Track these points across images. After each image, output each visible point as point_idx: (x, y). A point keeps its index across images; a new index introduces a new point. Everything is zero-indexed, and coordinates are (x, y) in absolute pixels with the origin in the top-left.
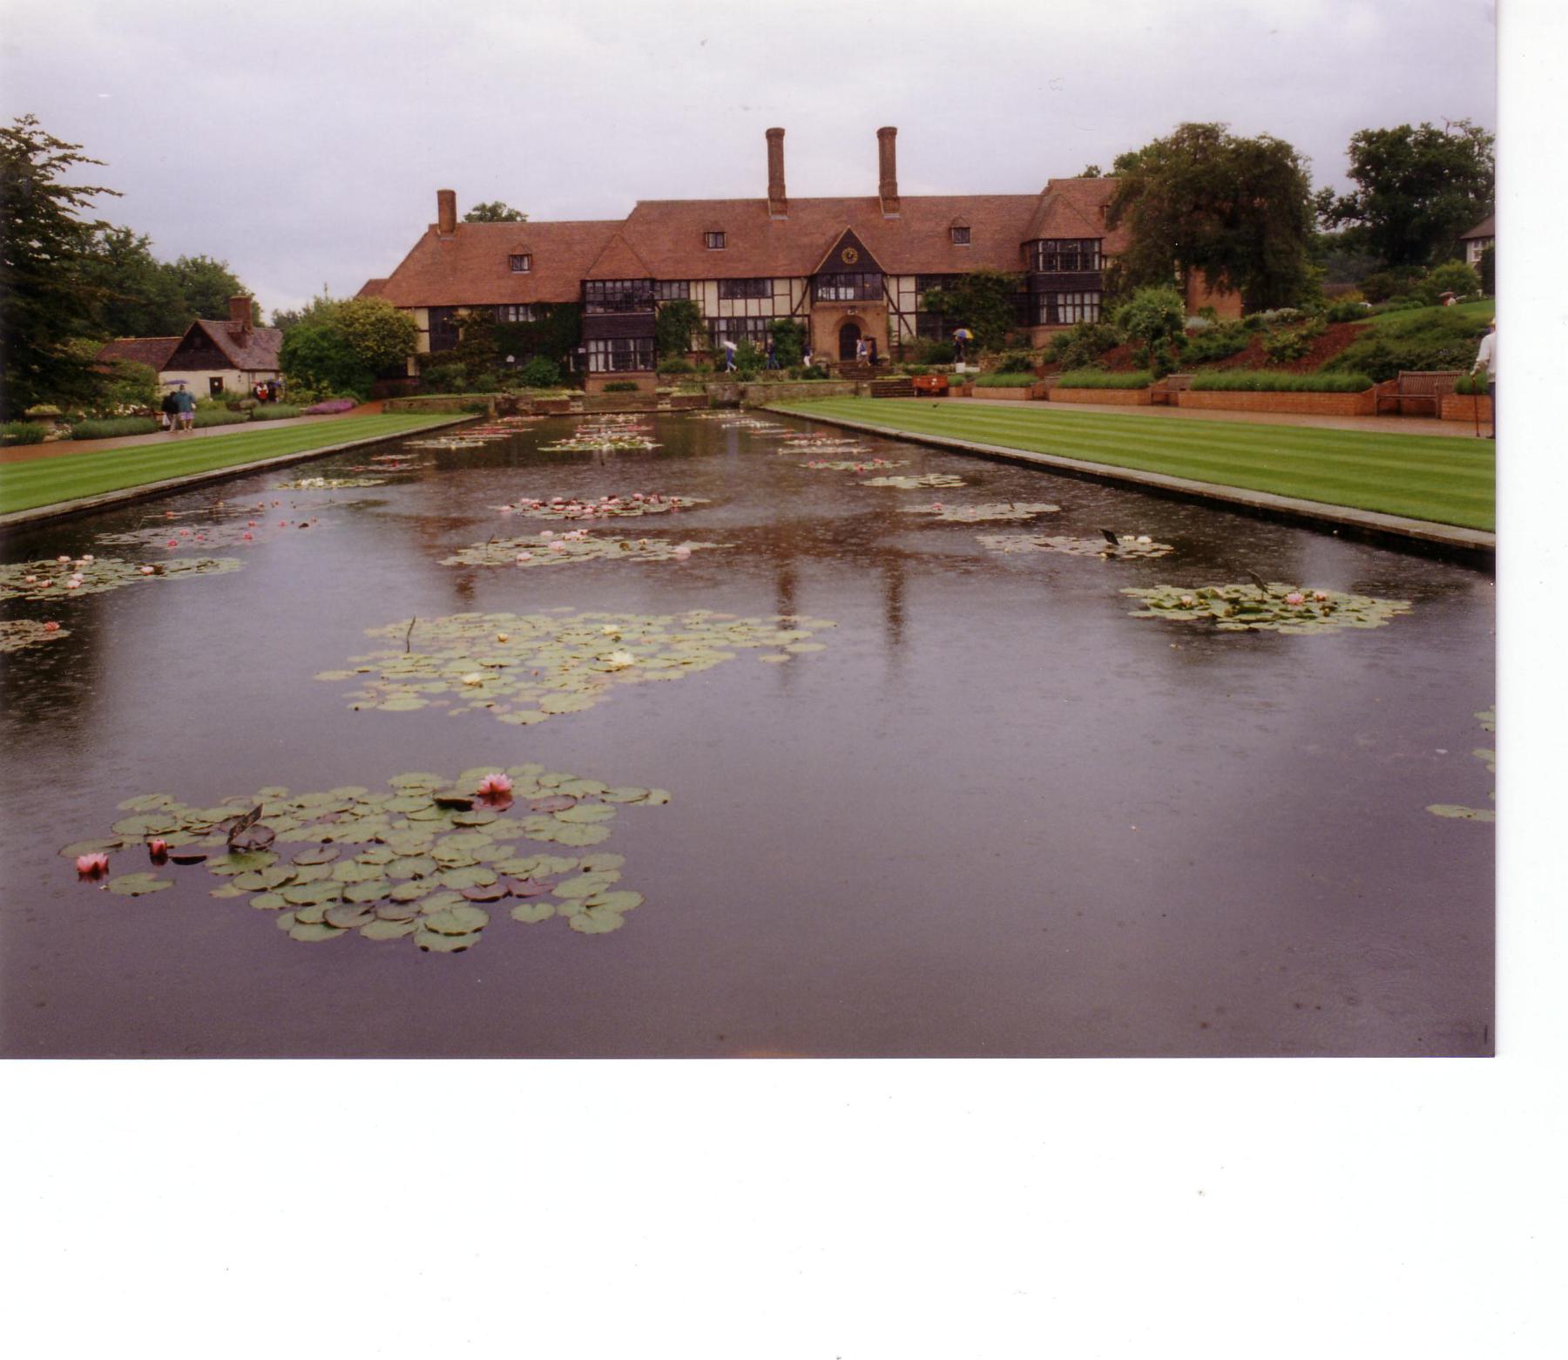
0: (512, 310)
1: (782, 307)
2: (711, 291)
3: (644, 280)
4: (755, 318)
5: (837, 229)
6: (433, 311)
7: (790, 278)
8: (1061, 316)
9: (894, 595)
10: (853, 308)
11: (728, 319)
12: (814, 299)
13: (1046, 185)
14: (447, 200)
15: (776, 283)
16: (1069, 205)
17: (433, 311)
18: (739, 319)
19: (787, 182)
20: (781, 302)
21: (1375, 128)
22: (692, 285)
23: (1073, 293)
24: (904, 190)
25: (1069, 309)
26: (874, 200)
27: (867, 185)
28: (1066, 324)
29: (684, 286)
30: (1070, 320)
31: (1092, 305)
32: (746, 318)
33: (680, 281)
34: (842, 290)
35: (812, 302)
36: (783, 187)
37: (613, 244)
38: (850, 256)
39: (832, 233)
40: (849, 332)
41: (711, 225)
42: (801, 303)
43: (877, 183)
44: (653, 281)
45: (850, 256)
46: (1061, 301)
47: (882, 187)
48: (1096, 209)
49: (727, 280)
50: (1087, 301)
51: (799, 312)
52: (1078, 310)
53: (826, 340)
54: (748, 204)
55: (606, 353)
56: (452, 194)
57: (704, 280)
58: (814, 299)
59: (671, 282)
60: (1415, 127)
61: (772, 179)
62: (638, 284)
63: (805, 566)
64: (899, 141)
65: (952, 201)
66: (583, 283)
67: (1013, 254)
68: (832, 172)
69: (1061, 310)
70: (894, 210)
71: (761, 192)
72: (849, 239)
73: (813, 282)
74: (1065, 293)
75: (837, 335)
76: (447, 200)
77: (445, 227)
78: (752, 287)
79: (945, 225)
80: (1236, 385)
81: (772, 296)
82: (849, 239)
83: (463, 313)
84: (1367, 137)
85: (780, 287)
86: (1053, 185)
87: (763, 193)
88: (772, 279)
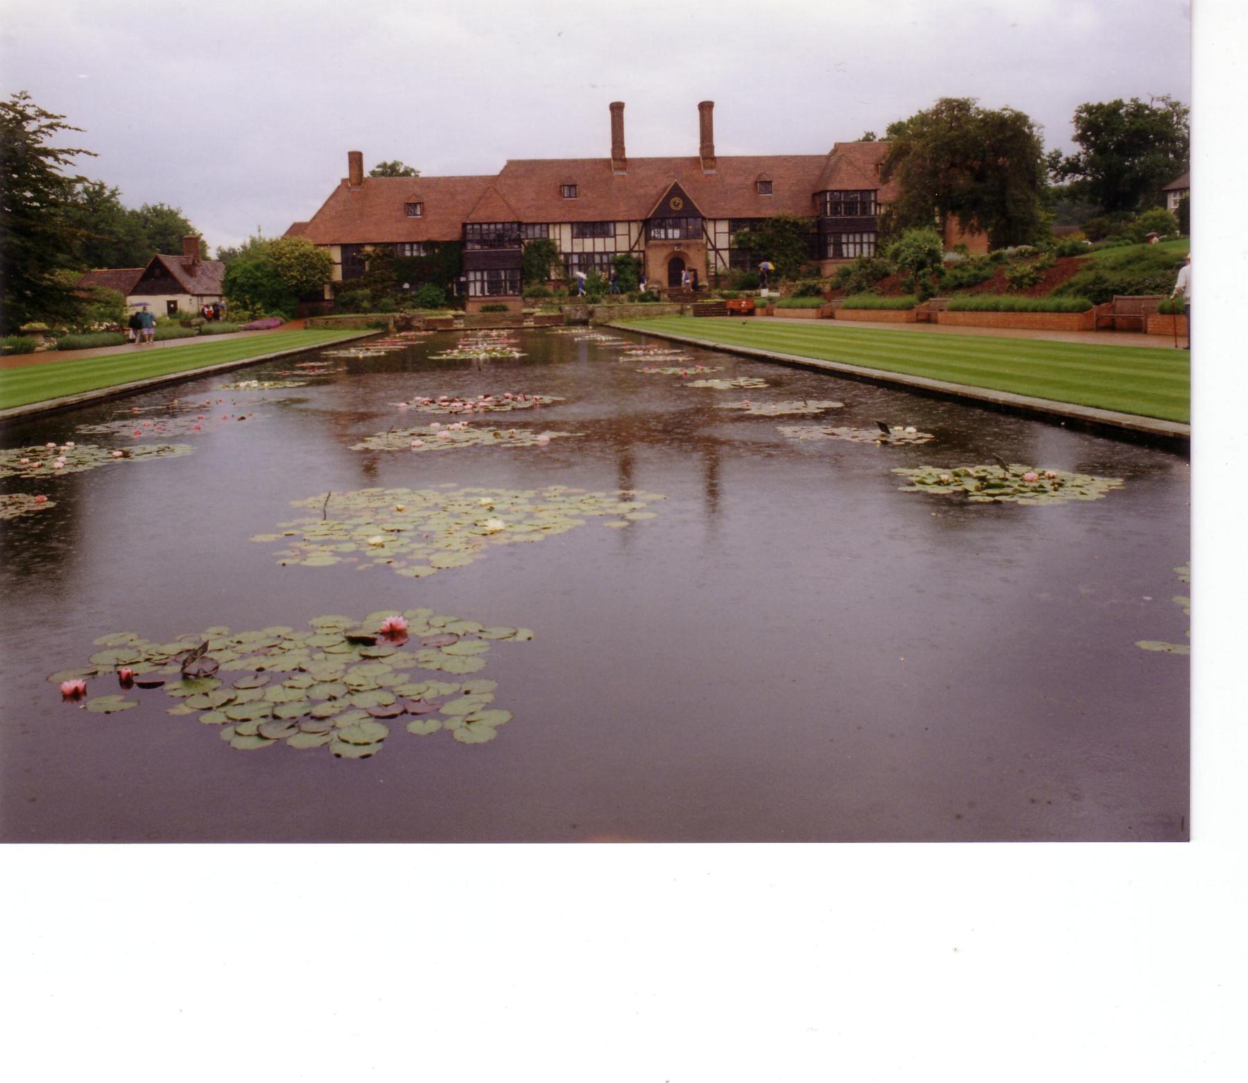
0: (407, 247)
1: (623, 244)
2: (566, 232)
3: (512, 223)
4: (601, 254)
5: (666, 182)
6: (345, 247)
7: (629, 222)
8: (845, 251)
9: (712, 474)
10: (679, 245)
11: (580, 254)
12: (648, 238)
13: (832, 147)
14: (356, 159)
15: (618, 225)
16: (850, 163)
17: (345, 247)
18: (588, 254)
19: (627, 145)
20: (622, 241)
21: (1094, 102)
22: (551, 227)
23: (854, 233)
24: (719, 151)
25: (851, 246)
26: (696, 160)
27: (690, 147)
28: (848, 258)
29: (544, 227)
30: (851, 255)
32: (594, 253)
33: (541, 224)
34: (670, 231)
35: (647, 241)
36: (623, 149)
37: (488, 195)
38: (677, 204)
39: (662, 185)
40: (676, 265)
41: (566, 179)
42: (637, 242)
43: (698, 146)
44: (520, 224)
45: (677, 204)
46: (844, 240)
47: (702, 149)
49: (578, 223)
50: (865, 239)
51: (636, 248)
52: (858, 247)
53: (657, 270)
54: (595, 162)
55: (482, 281)
56: (360, 154)
57: (560, 223)
58: (648, 238)
61: (614, 142)
62: (507, 226)
64: (716, 112)
65: (758, 160)
66: (464, 225)
67: (806, 203)
68: (662, 137)
69: (844, 247)
70: (712, 167)
71: (606, 153)
72: (676, 191)
73: (647, 224)
74: (848, 234)
75: (666, 267)
76: (356, 159)
77: (354, 181)
78: (598, 228)
79: (752, 179)
80: (984, 306)
81: (615, 236)
82: (676, 191)
83: (369, 249)
84: (1088, 109)
85: (621, 229)
87: (607, 154)
88: (615, 222)
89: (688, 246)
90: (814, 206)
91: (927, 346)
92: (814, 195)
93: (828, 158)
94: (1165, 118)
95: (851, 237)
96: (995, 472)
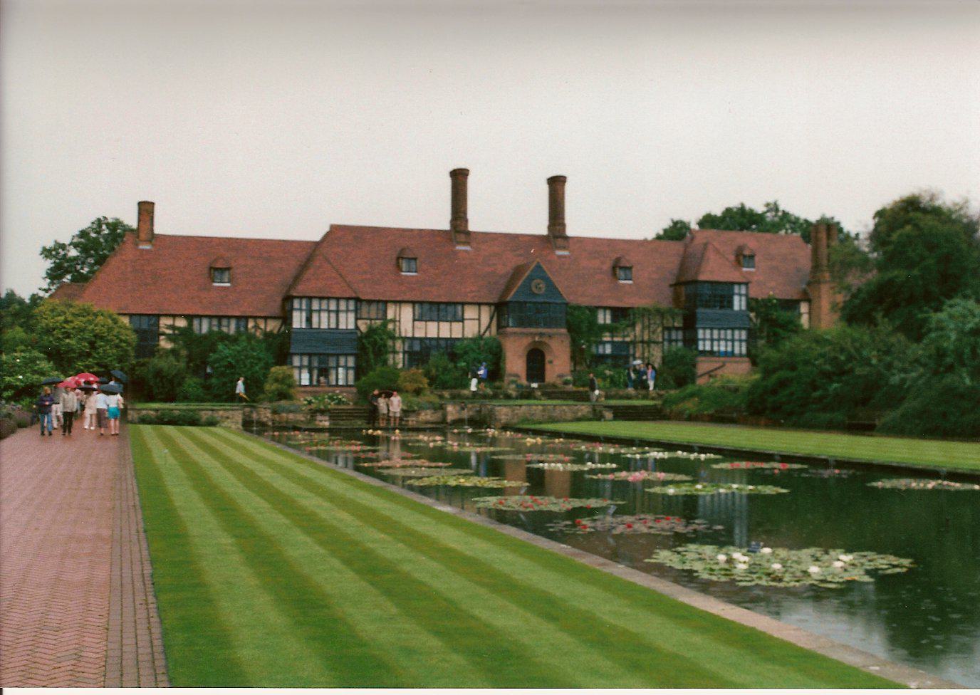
2: (407, 313)
7: (479, 304)
11: (421, 340)
13: (327, 229)
14: (146, 209)
15: (466, 307)
16: (717, 251)
20: (473, 324)
23: (726, 329)
24: (574, 227)
27: (538, 225)
31: (741, 341)
33: (378, 301)
34: (351, 326)
35: (499, 327)
36: (563, 225)
41: (402, 247)
42: (489, 327)
47: (550, 227)
49: (421, 303)
50: (315, 305)
53: (515, 364)
57: (401, 302)
63: (151, 656)
64: (569, 189)
67: (668, 292)
68: (507, 209)
70: (564, 248)
71: (442, 221)
73: (500, 309)
75: (525, 359)
81: (462, 320)
83: (775, 301)
85: (470, 313)
86: (337, 232)
87: (442, 221)
88: (463, 304)
89: (550, 336)
90: (283, 307)
94: (822, 218)
95: (716, 332)
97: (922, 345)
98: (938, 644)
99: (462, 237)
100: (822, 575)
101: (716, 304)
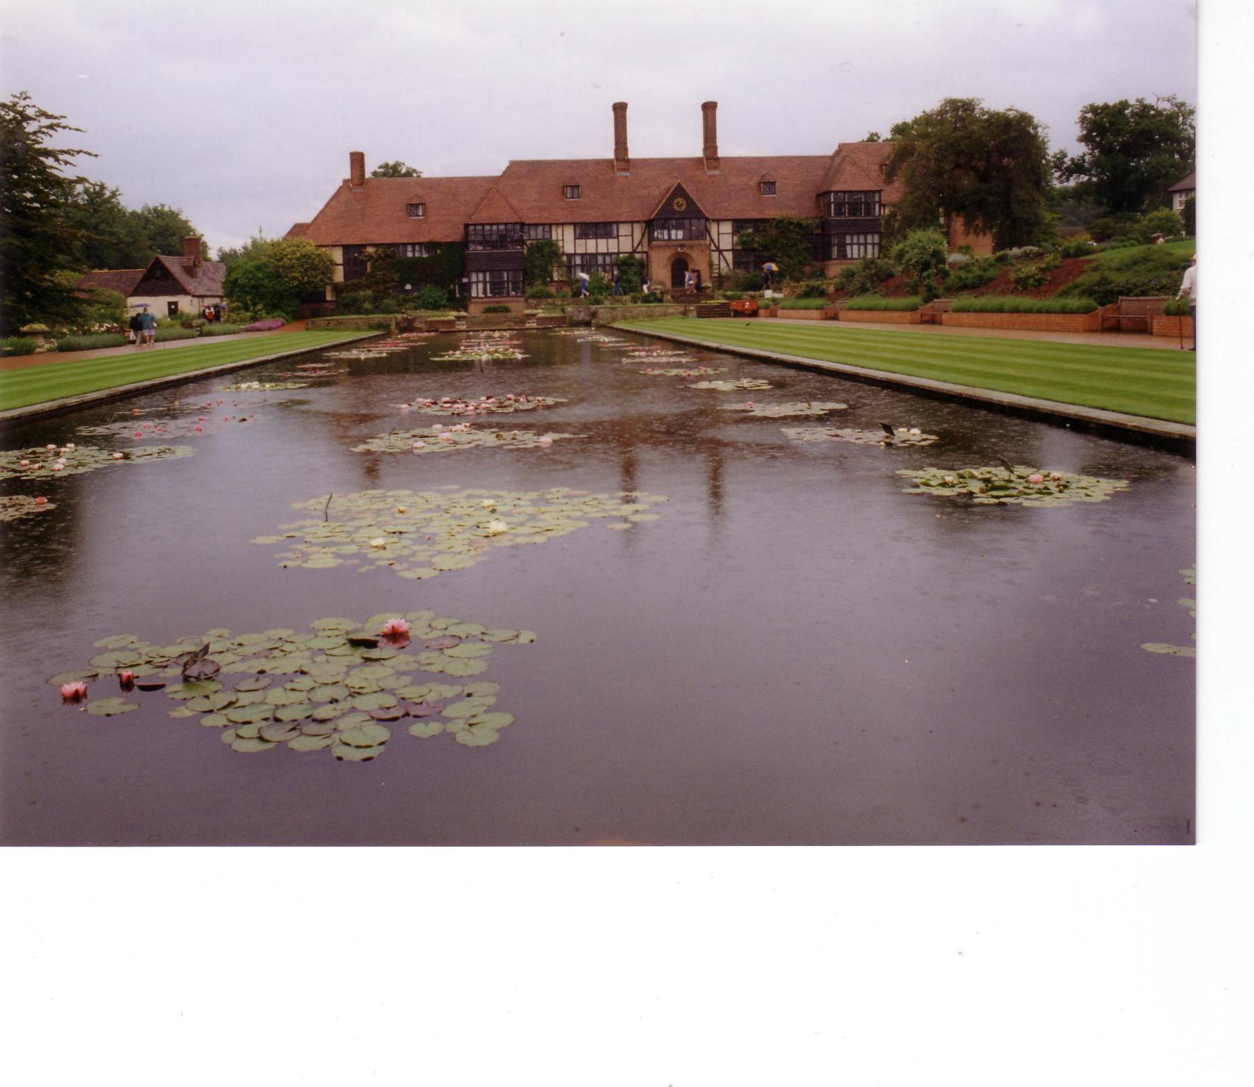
0: (409, 248)
1: (626, 245)
2: (569, 233)
3: (515, 224)
4: (604, 255)
5: (669, 183)
6: (346, 248)
7: (632, 222)
8: (849, 252)
9: (715, 476)
10: (682, 246)
11: (582, 255)
12: (651, 239)
13: (836, 148)
14: (357, 160)
15: (621, 226)
17: (346, 248)
19: (630, 146)
20: (625, 242)
21: (1100, 102)
22: (554, 228)
24: (723, 151)
25: (855, 247)
26: (699, 160)
27: (693, 148)
28: (852, 259)
29: (547, 228)
30: (856, 256)
32: (597, 254)
33: (543, 225)
35: (650, 242)
37: (490, 195)
38: (680, 204)
39: (666, 186)
40: (679, 266)
41: (568, 180)
42: (640, 242)
43: (702, 146)
44: (522, 225)
45: (680, 204)
46: (848, 241)
47: (705, 149)
48: (877, 167)
49: (581, 224)
50: (869, 240)
51: (639, 249)
52: (862, 247)
53: (660, 271)
54: (598, 163)
55: (485, 282)
56: (362, 155)
57: (563, 224)
58: (651, 239)
59: (536, 225)
60: (1132, 102)
62: (510, 227)
63: (644, 453)
64: (719, 112)
65: (761, 161)
66: (467, 226)
67: (810, 203)
68: (666, 137)
69: (848, 248)
70: (715, 168)
71: (609, 153)
72: (679, 191)
73: (650, 225)
74: (852, 235)
75: (669, 268)
76: (357, 160)
77: (356, 181)
78: (601, 229)
79: (756, 180)
81: (618, 237)
82: (679, 191)
84: (1093, 109)
85: (624, 230)
87: (610, 155)
88: (618, 223)
89: (691, 247)
91: (932, 347)
92: (818, 196)
93: (832, 158)
94: (1171, 119)
95: (855, 238)
96: (1000, 474)
97: (941, 247)
98: (911, 448)
99: (713, 163)
100: (203, 410)
101: (148, 243)
